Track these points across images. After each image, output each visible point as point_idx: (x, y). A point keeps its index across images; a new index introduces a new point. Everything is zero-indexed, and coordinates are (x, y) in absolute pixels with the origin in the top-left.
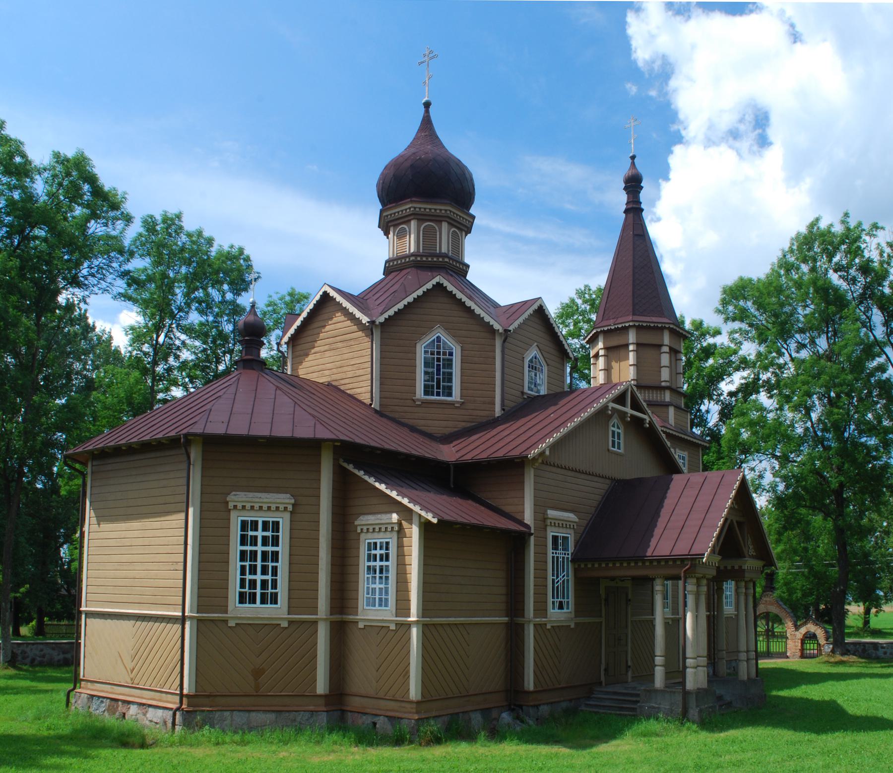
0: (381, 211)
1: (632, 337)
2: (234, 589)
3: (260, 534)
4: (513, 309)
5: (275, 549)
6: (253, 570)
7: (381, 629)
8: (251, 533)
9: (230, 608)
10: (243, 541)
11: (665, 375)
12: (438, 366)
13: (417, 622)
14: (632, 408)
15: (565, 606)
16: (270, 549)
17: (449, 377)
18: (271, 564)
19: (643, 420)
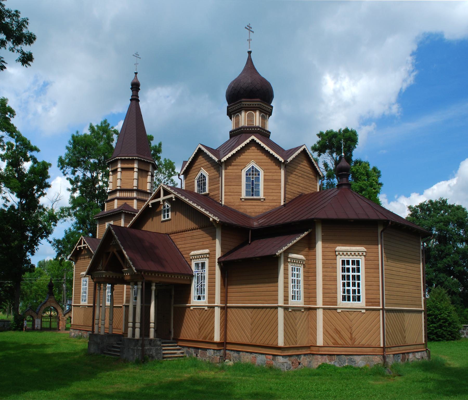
0: (228, 107)
1: (136, 166)
2: (340, 294)
4: (292, 151)
5: (358, 274)
6: (349, 285)
7: (200, 309)
9: (338, 303)
12: (253, 181)
16: (356, 274)
18: (357, 282)
19: (172, 198)
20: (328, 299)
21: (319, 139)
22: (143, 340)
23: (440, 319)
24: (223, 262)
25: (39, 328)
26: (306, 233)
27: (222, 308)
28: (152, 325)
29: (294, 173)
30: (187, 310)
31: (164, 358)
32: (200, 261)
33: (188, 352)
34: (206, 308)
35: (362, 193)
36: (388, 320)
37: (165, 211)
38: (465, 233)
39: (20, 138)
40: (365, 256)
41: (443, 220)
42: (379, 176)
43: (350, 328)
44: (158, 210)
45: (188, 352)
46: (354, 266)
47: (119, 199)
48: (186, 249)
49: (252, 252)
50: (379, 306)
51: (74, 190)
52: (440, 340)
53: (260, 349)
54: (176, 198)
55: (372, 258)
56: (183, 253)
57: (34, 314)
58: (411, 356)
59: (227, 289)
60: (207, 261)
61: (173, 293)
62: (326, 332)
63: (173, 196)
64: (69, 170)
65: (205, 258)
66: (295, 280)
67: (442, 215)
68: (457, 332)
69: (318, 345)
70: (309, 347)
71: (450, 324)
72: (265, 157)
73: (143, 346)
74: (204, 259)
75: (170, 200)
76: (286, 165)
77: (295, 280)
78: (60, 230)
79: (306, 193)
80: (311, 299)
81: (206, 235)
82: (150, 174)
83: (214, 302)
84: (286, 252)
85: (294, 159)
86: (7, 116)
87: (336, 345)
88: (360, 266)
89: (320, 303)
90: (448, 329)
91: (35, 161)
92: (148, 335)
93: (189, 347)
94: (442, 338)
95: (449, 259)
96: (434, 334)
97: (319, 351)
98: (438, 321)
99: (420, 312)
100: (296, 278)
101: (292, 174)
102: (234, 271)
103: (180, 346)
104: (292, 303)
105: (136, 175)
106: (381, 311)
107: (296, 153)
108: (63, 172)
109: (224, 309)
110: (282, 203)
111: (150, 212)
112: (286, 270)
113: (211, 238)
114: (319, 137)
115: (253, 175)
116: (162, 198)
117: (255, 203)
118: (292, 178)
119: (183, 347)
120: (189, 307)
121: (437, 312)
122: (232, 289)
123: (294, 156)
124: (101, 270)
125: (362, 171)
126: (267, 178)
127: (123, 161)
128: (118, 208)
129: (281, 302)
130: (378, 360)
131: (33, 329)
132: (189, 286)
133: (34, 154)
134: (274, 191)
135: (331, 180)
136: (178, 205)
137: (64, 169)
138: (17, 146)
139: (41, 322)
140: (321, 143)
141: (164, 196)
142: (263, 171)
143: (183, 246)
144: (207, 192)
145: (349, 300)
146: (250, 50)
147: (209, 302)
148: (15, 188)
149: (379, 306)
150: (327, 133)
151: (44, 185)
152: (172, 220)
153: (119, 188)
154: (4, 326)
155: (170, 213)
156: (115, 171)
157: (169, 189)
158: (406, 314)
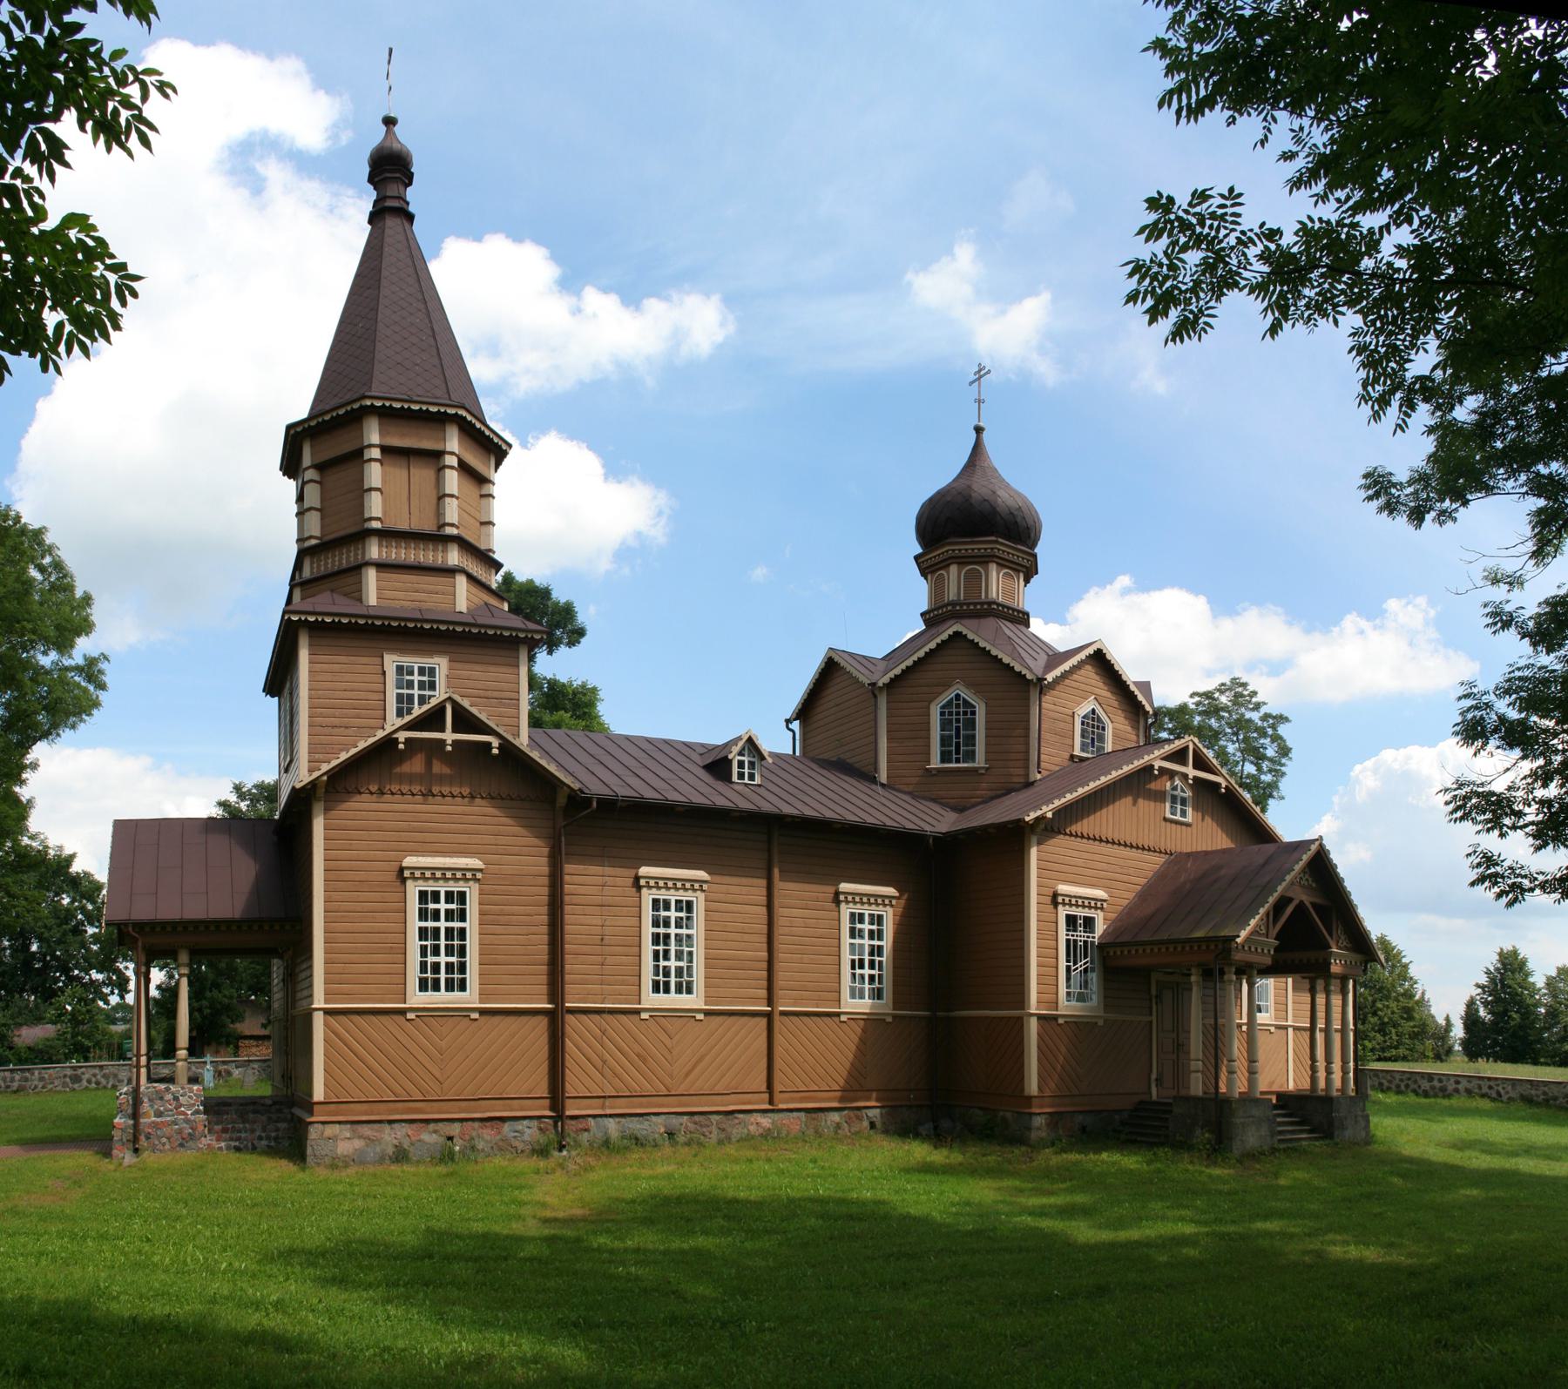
5: (423, 924)
6: (436, 952)
10: (656, 924)
11: (452, 512)
12: (958, 729)
14: (1195, 767)
16: (456, 925)
17: (971, 740)
19: (1218, 785)
107: (1074, 661)
142: (983, 706)
145: (667, 991)
147: (1276, 1018)
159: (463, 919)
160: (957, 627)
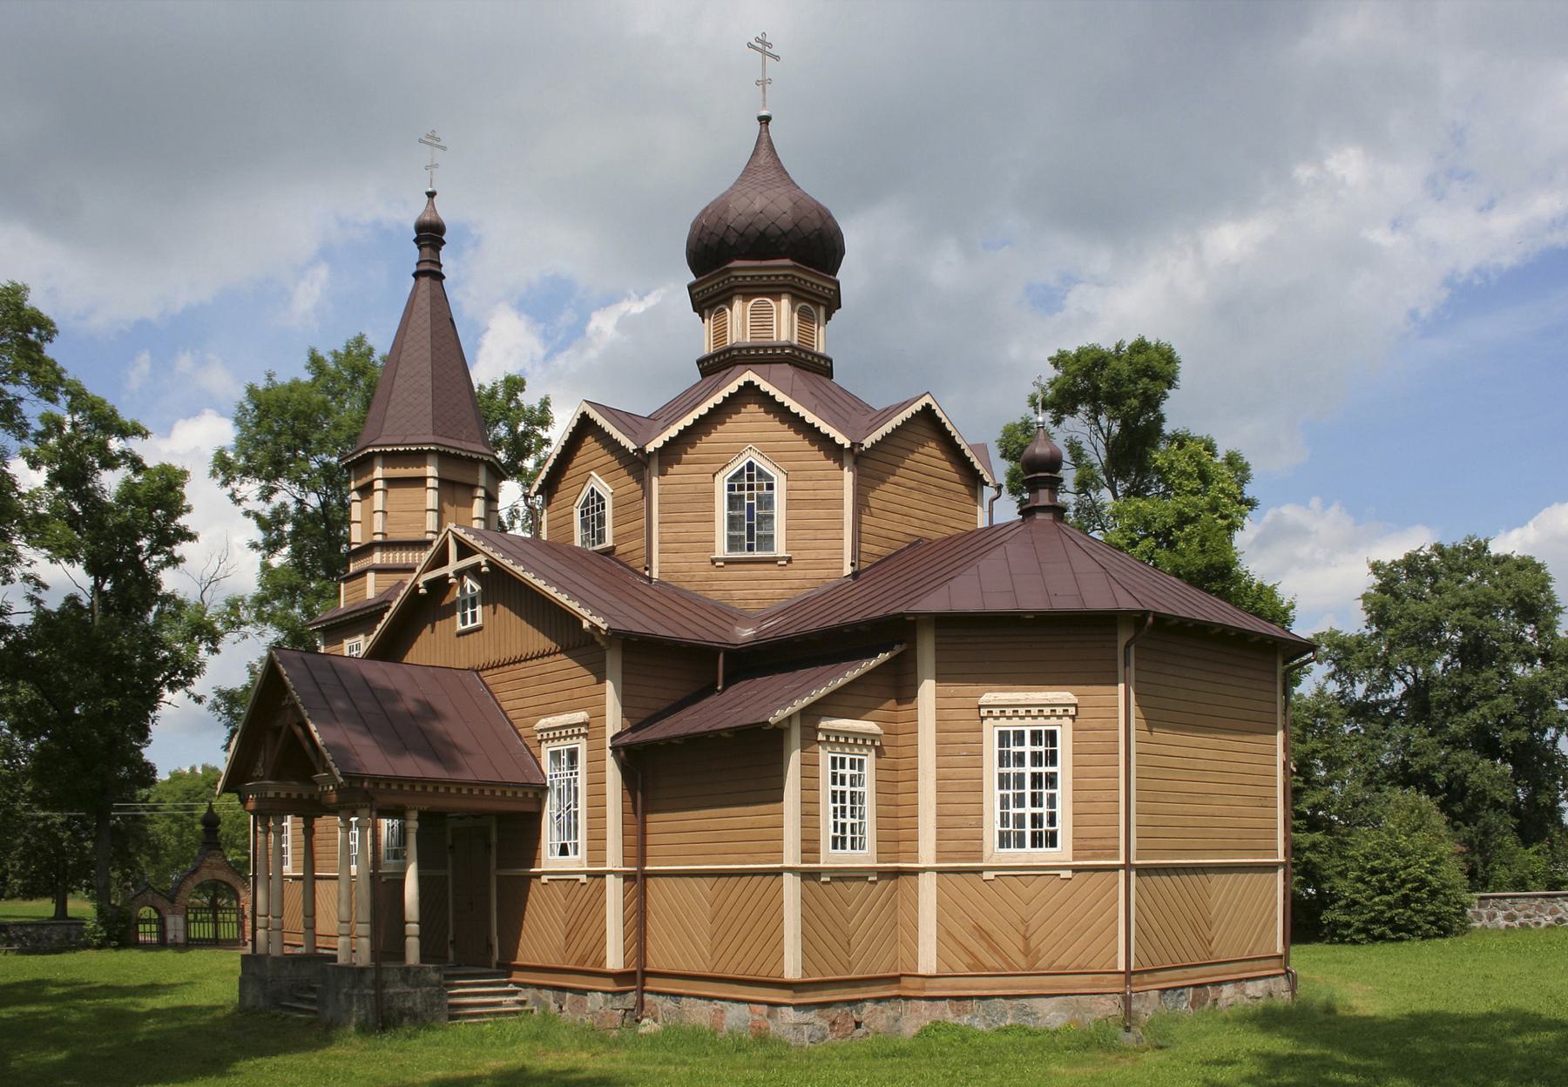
1: (431, 470)
3: (1028, 748)
6: (1020, 801)
7: (566, 879)
8: (1042, 749)
9: (987, 852)
12: (751, 506)
13: (1284, 865)
15: (571, 850)
16: (1044, 769)
18: (1046, 792)
19: (478, 565)
20: (952, 845)
21: (1052, 373)
22: (378, 970)
23: (1404, 882)
24: (628, 748)
25: (181, 939)
26: (883, 657)
27: (627, 877)
28: (413, 928)
29: (892, 479)
30: (534, 884)
31: (452, 1017)
32: (563, 746)
33: (538, 1001)
34: (583, 878)
35: (1182, 530)
36: (1146, 894)
37: (464, 602)
38: (1539, 636)
39: (79, 400)
40: (1073, 717)
41: (1471, 600)
42: (1243, 481)
43: (1023, 921)
44: (447, 601)
45: (538, 1001)
46: (1037, 749)
47: (379, 570)
48: (524, 712)
49: (705, 718)
50: (1117, 857)
51: (272, 546)
52: (1401, 939)
53: (736, 987)
54: (490, 563)
55: (1096, 723)
56: (517, 723)
57: (162, 903)
58: (1228, 991)
59: (644, 822)
60: (582, 746)
61: (494, 838)
62: (945, 934)
63: (480, 559)
64: (250, 488)
65: (578, 736)
66: (843, 793)
67: (1472, 587)
68: (1457, 915)
69: (921, 971)
70: (896, 979)
71: (1434, 893)
72: (791, 434)
73: (379, 984)
74: (572, 742)
75: (474, 571)
76: (857, 458)
77: (843, 793)
78: (233, 663)
79: (935, 536)
80: (903, 846)
81: (582, 670)
82: (481, 493)
83: (604, 862)
84: (811, 715)
85: (887, 437)
86: (32, 337)
87: (978, 969)
88: (1058, 748)
89: (927, 855)
90: (1429, 907)
91: (137, 464)
92: (401, 955)
93: (540, 987)
94: (1410, 932)
95: (1485, 710)
96: (1385, 923)
97: (924, 989)
98: (1399, 887)
99: (1273, 868)
100: (847, 788)
101: (884, 482)
102: (658, 773)
103: (516, 984)
104: (830, 858)
105: (431, 498)
106: (1122, 872)
107: (897, 420)
108: (232, 496)
109: (637, 880)
110: (848, 570)
111: (427, 606)
112: (810, 766)
113: (593, 679)
114: (1056, 367)
115: (751, 487)
116: (454, 565)
117: (759, 571)
118: (882, 495)
119: (525, 985)
120: (538, 876)
121: (1397, 862)
122: (658, 823)
123: (887, 428)
124: (262, 778)
125: (1183, 464)
126: (796, 495)
127: (391, 458)
128: (379, 595)
129: (791, 856)
130: (1108, 1007)
131: (162, 944)
132: (537, 817)
133: (135, 445)
134: (819, 534)
135: (1093, 494)
136: (500, 586)
137: (235, 485)
138: (74, 425)
139: (187, 922)
140: (1057, 386)
141: (460, 558)
143: (518, 703)
144: (609, 542)
145: (1021, 844)
146: (764, 113)
147: (590, 862)
148: (60, 547)
149: (1117, 857)
150: (1081, 352)
151: (169, 538)
152: (486, 630)
153: (379, 538)
154: (68, 936)
155: (479, 609)
156: (366, 491)
157: (469, 538)
158: (1217, 879)
159: (1053, 762)
160: (749, 376)
